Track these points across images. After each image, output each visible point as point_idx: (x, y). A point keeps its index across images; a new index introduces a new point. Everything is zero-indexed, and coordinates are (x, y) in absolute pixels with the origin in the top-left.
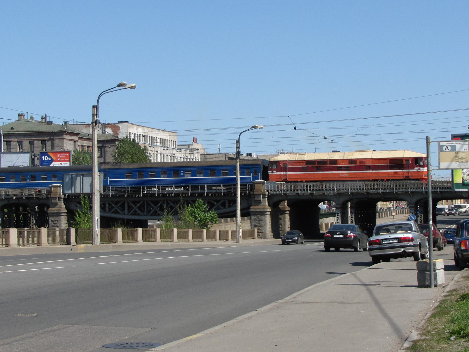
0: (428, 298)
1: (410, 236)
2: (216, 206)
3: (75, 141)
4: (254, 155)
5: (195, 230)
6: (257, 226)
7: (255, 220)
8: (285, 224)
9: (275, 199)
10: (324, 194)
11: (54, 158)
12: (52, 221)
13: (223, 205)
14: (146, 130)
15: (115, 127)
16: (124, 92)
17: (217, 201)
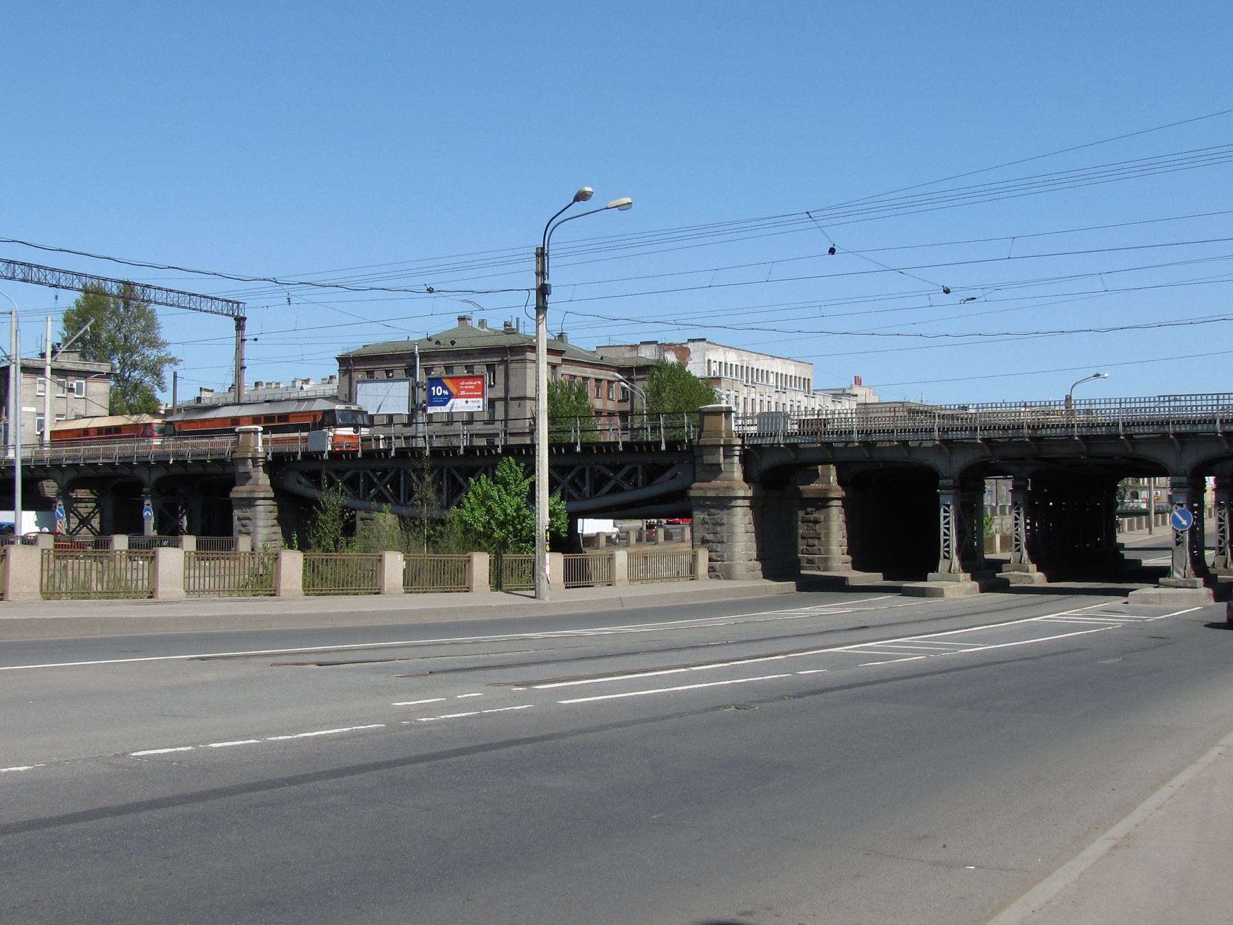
2: (612, 483)
5: (414, 555)
6: (708, 541)
7: (704, 522)
8: (828, 535)
10: (905, 443)
11: (454, 391)
12: (239, 519)
14: (746, 356)
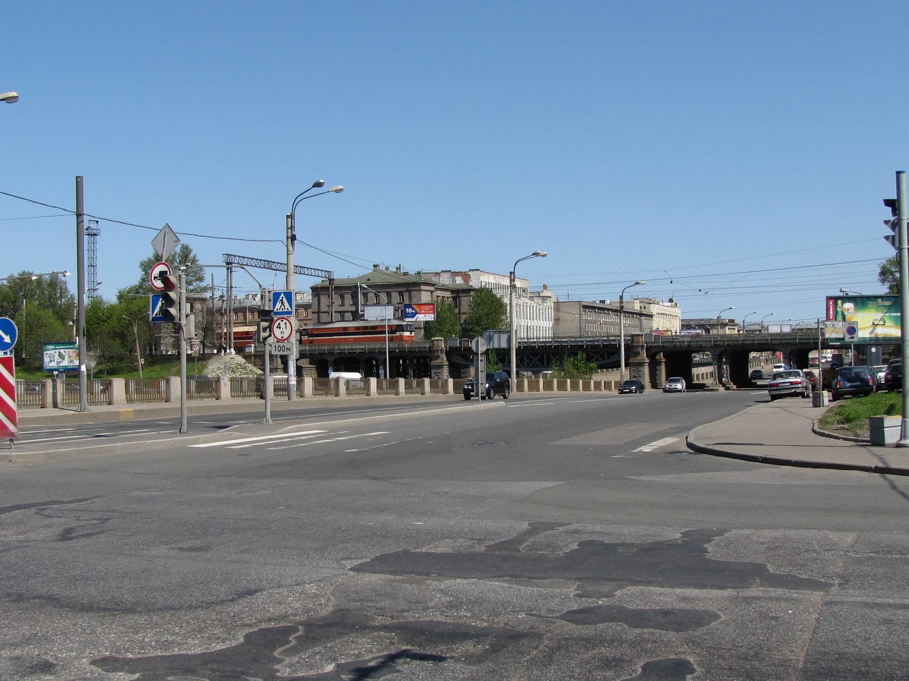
0: (819, 412)
1: (799, 380)
3: (432, 292)
4: (608, 302)
9: (653, 351)
11: (418, 310)
13: (602, 356)
15: (466, 276)
16: (536, 258)
17: (596, 353)
